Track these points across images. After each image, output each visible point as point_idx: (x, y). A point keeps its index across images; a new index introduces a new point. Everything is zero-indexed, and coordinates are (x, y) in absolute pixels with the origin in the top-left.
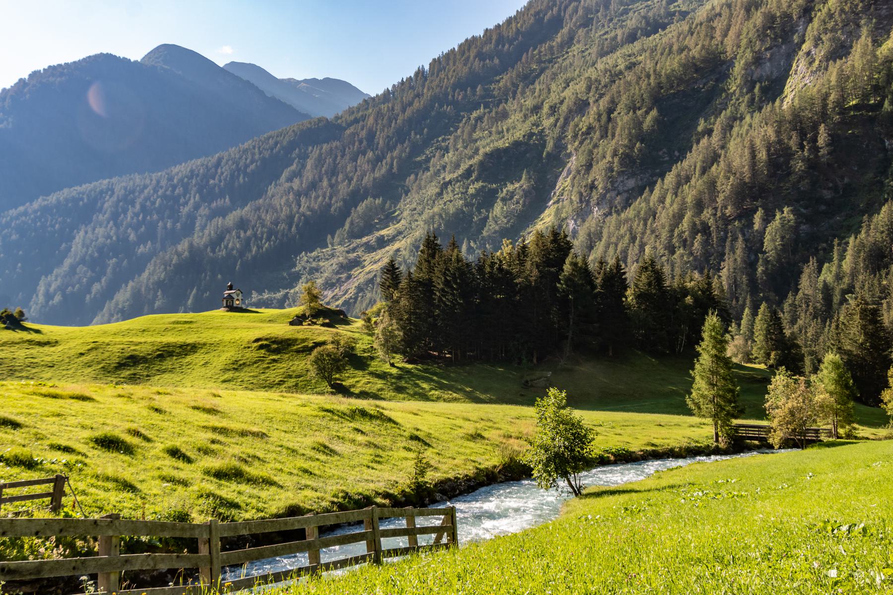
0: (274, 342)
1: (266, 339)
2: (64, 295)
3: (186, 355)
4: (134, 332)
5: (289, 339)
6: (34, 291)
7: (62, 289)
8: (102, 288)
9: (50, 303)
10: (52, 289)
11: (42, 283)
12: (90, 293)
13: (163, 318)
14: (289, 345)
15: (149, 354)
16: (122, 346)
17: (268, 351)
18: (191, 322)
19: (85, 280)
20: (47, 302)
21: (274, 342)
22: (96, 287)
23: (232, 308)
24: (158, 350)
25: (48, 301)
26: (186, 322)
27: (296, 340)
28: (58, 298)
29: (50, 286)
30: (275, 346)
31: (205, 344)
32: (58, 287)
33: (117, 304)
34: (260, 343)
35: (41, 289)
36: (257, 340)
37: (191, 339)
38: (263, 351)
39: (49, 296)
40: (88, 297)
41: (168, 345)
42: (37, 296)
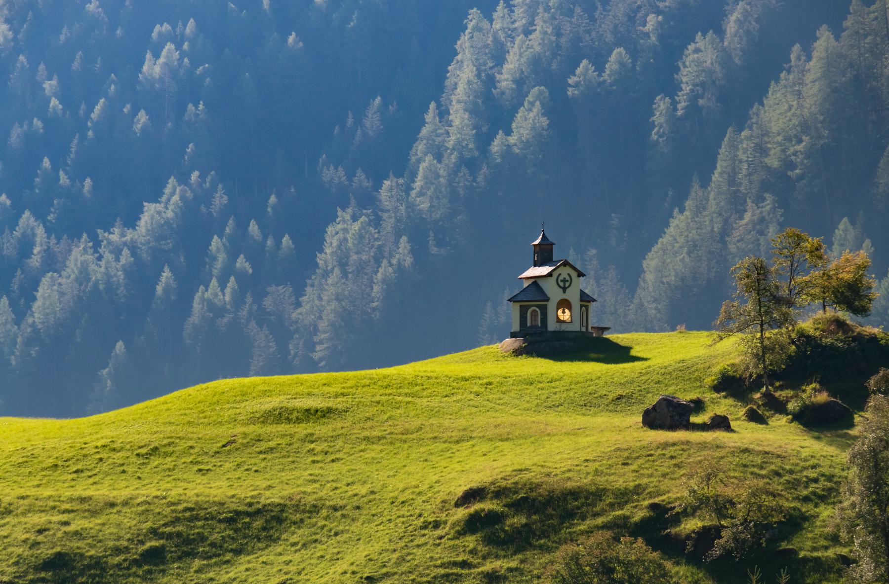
0: (518, 506)
1: (499, 493)
2: (558, 107)
3: (238, 552)
4: (118, 457)
5: (575, 494)
6: (435, 87)
7: (548, 73)
8: (725, 59)
9: (496, 146)
10: (505, 79)
11: (466, 47)
12: (671, 88)
13: (98, 424)
14: (569, 515)
15: (117, 551)
16: (39, 519)
17: (489, 540)
18: (326, 413)
19: (652, 20)
20: (484, 140)
21: (518, 506)
22: (700, 57)
23: (540, 341)
24: (154, 533)
25: (489, 138)
26: (309, 414)
27: (599, 494)
28: (528, 121)
29: (499, 59)
30: (519, 520)
31: (315, 509)
32: (536, 62)
33: (762, 150)
34: (477, 506)
35: (463, 76)
36: (472, 495)
37: (271, 486)
38: (471, 541)
39: (493, 113)
40: (661, 105)
41: (194, 513)
42: (443, 114)
